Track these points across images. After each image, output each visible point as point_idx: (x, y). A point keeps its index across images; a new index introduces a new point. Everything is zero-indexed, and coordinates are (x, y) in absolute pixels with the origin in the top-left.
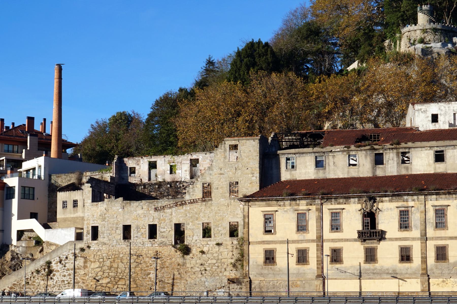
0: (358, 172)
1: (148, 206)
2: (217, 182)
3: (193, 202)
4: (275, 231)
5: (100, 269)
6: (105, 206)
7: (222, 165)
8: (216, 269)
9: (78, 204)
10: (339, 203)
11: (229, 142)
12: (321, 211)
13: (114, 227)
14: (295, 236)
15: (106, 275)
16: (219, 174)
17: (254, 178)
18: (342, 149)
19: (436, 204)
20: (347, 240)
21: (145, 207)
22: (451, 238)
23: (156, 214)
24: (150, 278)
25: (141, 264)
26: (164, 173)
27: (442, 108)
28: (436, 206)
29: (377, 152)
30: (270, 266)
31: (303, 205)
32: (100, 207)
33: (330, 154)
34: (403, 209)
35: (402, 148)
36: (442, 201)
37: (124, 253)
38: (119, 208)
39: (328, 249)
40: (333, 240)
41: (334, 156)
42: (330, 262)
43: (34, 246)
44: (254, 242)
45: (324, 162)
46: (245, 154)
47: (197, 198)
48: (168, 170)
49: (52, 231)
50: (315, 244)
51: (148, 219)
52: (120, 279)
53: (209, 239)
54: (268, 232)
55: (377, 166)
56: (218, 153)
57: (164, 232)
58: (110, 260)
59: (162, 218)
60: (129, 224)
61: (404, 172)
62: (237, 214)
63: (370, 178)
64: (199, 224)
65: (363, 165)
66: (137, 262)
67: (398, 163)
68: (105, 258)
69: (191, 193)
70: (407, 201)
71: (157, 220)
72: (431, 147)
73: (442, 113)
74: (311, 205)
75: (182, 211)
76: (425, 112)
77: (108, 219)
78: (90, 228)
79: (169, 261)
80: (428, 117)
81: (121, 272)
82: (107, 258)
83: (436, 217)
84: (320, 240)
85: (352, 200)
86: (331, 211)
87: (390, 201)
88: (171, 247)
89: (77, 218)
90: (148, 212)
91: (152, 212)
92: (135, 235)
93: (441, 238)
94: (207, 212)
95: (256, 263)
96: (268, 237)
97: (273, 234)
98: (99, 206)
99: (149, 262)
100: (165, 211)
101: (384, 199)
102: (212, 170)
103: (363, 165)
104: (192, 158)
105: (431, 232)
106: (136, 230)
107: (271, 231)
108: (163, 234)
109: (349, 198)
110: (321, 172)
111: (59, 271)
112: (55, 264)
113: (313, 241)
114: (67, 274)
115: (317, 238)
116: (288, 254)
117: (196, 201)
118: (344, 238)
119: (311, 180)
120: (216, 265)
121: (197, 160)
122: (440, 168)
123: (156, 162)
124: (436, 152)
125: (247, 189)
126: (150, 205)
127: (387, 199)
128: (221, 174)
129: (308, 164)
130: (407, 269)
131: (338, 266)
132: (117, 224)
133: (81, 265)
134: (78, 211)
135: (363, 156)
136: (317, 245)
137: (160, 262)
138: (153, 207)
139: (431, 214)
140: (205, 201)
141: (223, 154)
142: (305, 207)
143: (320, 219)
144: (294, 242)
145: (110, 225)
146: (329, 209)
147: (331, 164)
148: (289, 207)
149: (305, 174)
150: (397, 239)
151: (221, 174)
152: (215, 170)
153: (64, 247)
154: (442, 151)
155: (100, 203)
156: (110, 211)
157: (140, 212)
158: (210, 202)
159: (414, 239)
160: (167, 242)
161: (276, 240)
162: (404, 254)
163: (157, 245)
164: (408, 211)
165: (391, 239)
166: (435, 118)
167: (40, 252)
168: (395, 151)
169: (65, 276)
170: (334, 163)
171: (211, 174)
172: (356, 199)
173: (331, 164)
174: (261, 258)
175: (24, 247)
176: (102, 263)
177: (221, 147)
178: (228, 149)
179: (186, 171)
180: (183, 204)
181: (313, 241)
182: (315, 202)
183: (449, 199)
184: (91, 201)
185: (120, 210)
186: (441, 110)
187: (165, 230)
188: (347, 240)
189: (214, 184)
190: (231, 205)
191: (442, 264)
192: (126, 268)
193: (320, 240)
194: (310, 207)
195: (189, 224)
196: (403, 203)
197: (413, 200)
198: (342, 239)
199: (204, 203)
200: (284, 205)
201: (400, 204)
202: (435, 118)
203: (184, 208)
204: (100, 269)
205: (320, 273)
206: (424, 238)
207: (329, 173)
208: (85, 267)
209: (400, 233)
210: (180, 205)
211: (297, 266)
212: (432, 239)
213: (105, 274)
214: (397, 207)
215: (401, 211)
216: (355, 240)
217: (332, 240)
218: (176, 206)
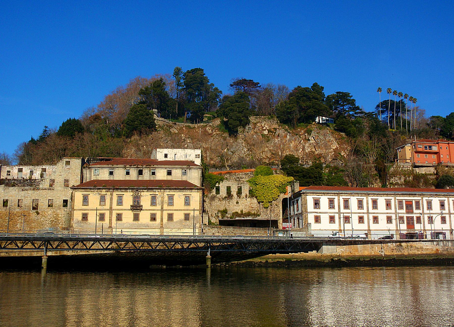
8: (54, 223)
9: (197, 158)
11: (65, 160)
12: (112, 195)
14: (183, 207)
20: (125, 210)
22: (175, 210)
25: (12, 219)
27: (169, 151)
28: (169, 195)
31: (104, 192)
35: (151, 168)
36: (172, 193)
40: (118, 210)
45: (114, 173)
50: (109, 211)
53: (51, 208)
55: (140, 176)
70: (155, 192)
74: (108, 192)
83: (169, 200)
84: (111, 209)
93: (187, 210)
95: (78, 220)
96: (186, 207)
105: (165, 207)
109: (127, 189)
113: (108, 210)
116: (97, 215)
120: (55, 221)
139: (166, 198)
143: (111, 199)
144: (99, 210)
150: (149, 210)
154: (171, 170)
159: (158, 210)
162: (153, 217)
164: (155, 197)
165: (146, 210)
166: (166, 156)
168: (148, 169)
174: (80, 218)
177: (61, 162)
178: (65, 163)
180: (38, 189)
181: (108, 210)
188: (125, 210)
190: (64, 191)
193: (339, 213)
194: (107, 193)
196: (153, 193)
197: (158, 192)
201: (152, 193)
202: (166, 156)
205: (111, 226)
206: (162, 210)
212: (166, 210)
215: (152, 196)
216: (129, 210)
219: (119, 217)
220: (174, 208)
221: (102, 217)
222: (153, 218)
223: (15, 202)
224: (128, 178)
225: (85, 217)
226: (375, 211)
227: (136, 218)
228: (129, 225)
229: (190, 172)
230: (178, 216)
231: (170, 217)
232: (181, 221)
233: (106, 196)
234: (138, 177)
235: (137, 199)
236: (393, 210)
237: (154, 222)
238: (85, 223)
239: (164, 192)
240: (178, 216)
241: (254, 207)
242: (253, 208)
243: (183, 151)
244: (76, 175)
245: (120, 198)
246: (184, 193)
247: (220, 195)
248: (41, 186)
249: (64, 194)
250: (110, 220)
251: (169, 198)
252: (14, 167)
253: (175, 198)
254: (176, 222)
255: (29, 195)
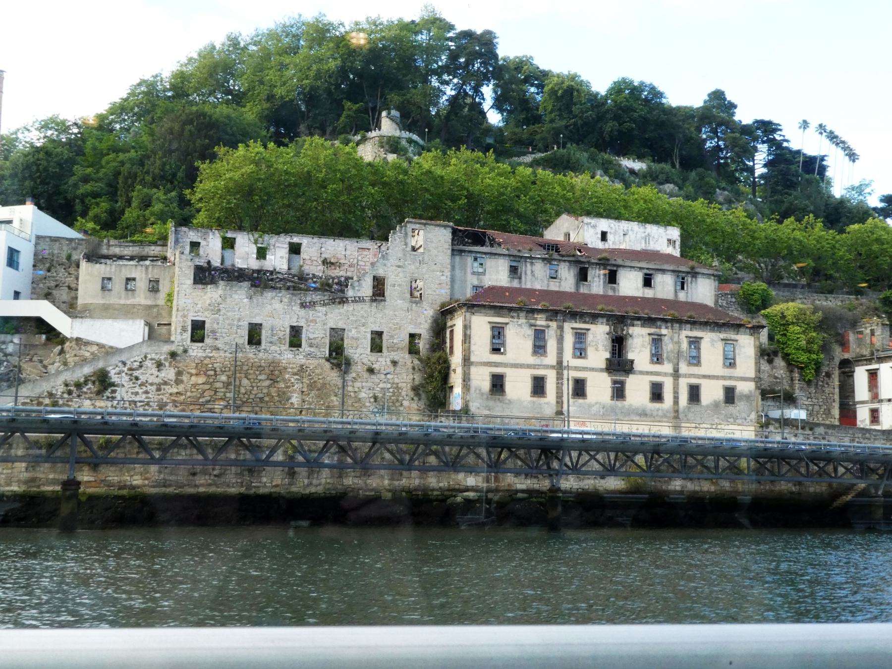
0: (560, 286)
1: (291, 299)
2: (393, 277)
3: (359, 300)
4: (505, 350)
5: (208, 387)
6: (220, 292)
7: (400, 255)
8: (391, 396)
10: (585, 322)
12: (561, 328)
13: (233, 325)
15: (220, 395)
16: (396, 266)
17: (444, 278)
18: (543, 256)
19: (690, 335)
20: (592, 369)
21: (285, 300)
22: (705, 377)
23: (302, 312)
24: (292, 403)
25: (277, 382)
26: (246, 258)
27: (612, 225)
28: (690, 337)
29: (582, 266)
30: (497, 397)
32: (208, 293)
33: (528, 260)
34: (656, 337)
37: (250, 365)
38: (244, 296)
39: (722, 387)
41: (532, 264)
42: (572, 395)
43: (45, 344)
44: (478, 363)
46: (433, 245)
47: (364, 295)
48: (253, 253)
49: (92, 323)
51: (291, 318)
52: (244, 402)
54: (496, 350)
56: (397, 238)
57: (315, 338)
58: (228, 373)
59: (311, 318)
60: (259, 322)
61: (610, 293)
62: (420, 324)
63: (571, 293)
64: (365, 332)
65: (566, 279)
66: (271, 380)
67: (604, 282)
68: (218, 369)
69: (357, 288)
71: (304, 320)
72: (641, 268)
73: (612, 231)
75: (342, 310)
76: (594, 227)
77: (224, 311)
78: (189, 323)
79: (321, 381)
80: (597, 233)
81: (246, 393)
82: (221, 371)
85: (600, 320)
86: (575, 331)
87: (643, 326)
88: (324, 361)
89: (134, 306)
90: (290, 307)
91: (297, 308)
92: (269, 340)
93: (730, 378)
94: (379, 315)
96: (496, 358)
97: (502, 354)
98: (209, 290)
99: (290, 380)
100: (316, 308)
101: (636, 322)
102: (388, 260)
103: (566, 279)
104: (291, 241)
106: (270, 332)
107: (500, 350)
108: (313, 341)
110: (516, 281)
111: (123, 386)
112: (115, 374)
114: (142, 390)
115: (557, 363)
117: (363, 299)
118: (589, 366)
119: (501, 288)
121: (299, 245)
122: (649, 293)
123: (235, 239)
124: (646, 274)
125: (435, 291)
126: (294, 298)
127: (639, 322)
128: (399, 267)
129: (500, 268)
130: (658, 410)
131: (581, 401)
132: (239, 320)
133: (171, 378)
134: (136, 295)
135: (567, 267)
136: (558, 373)
137: (308, 382)
138: (299, 302)
140: (376, 300)
141: (403, 240)
142: (543, 323)
143: (560, 340)
145: (227, 322)
146: (572, 328)
147: (529, 272)
148: (524, 321)
149: (497, 281)
150: (648, 373)
151: (399, 267)
152: (391, 260)
153: (135, 348)
155: (209, 286)
156: (228, 299)
157: (277, 305)
158: (383, 303)
159: (666, 374)
160: (318, 354)
161: (506, 361)
163: (302, 357)
164: (661, 340)
166: (604, 236)
167: (60, 354)
169: (137, 394)
170: (532, 272)
171: (385, 265)
172: (605, 320)
173: (529, 272)
174: (486, 385)
175: (17, 344)
176: (213, 377)
177: (401, 230)
179: (282, 257)
180: (343, 301)
182: (557, 317)
183: (703, 331)
184: (192, 281)
185: (246, 300)
186: (611, 228)
187: (315, 336)
188: (592, 369)
189: (389, 280)
190: (411, 310)
191: (695, 408)
192: (253, 387)
193: (560, 366)
194: (550, 323)
195: (350, 331)
197: (667, 328)
198: (587, 368)
199: (375, 304)
200: (518, 317)
201: (652, 330)
202: (604, 236)
203: (345, 307)
204: (208, 387)
205: (560, 409)
206: (676, 374)
207: (525, 284)
208: (178, 382)
209: (652, 366)
210: (340, 303)
211: (532, 399)
212: (685, 376)
213: (218, 394)
214: (649, 334)
216: (601, 370)
217: (576, 367)
218: (333, 303)
219: (579, 388)
220: (703, 370)
221: (538, 386)
222: (657, 394)
223: (281, 334)
224: (554, 286)
225: (498, 384)
226: (540, 372)
227: (619, 392)
228: (601, 410)
229: (694, 284)
230: (712, 393)
231: (694, 393)
232: (716, 405)
233: (546, 331)
234: (577, 286)
235: (618, 343)
236: (551, 358)
237: (657, 405)
238: (499, 399)
239: (680, 329)
240: (712, 393)
241: (780, 376)
242: (776, 378)
243: (642, 229)
244: (439, 269)
245: (580, 336)
246: (722, 336)
247: (305, 326)
248: (350, 293)
249: (411, 320)
250: (559, 395)
251: (690, 343)
252: (211, 234)
253: (704, 345)
254: (707, 407)
255: (319, 317)
